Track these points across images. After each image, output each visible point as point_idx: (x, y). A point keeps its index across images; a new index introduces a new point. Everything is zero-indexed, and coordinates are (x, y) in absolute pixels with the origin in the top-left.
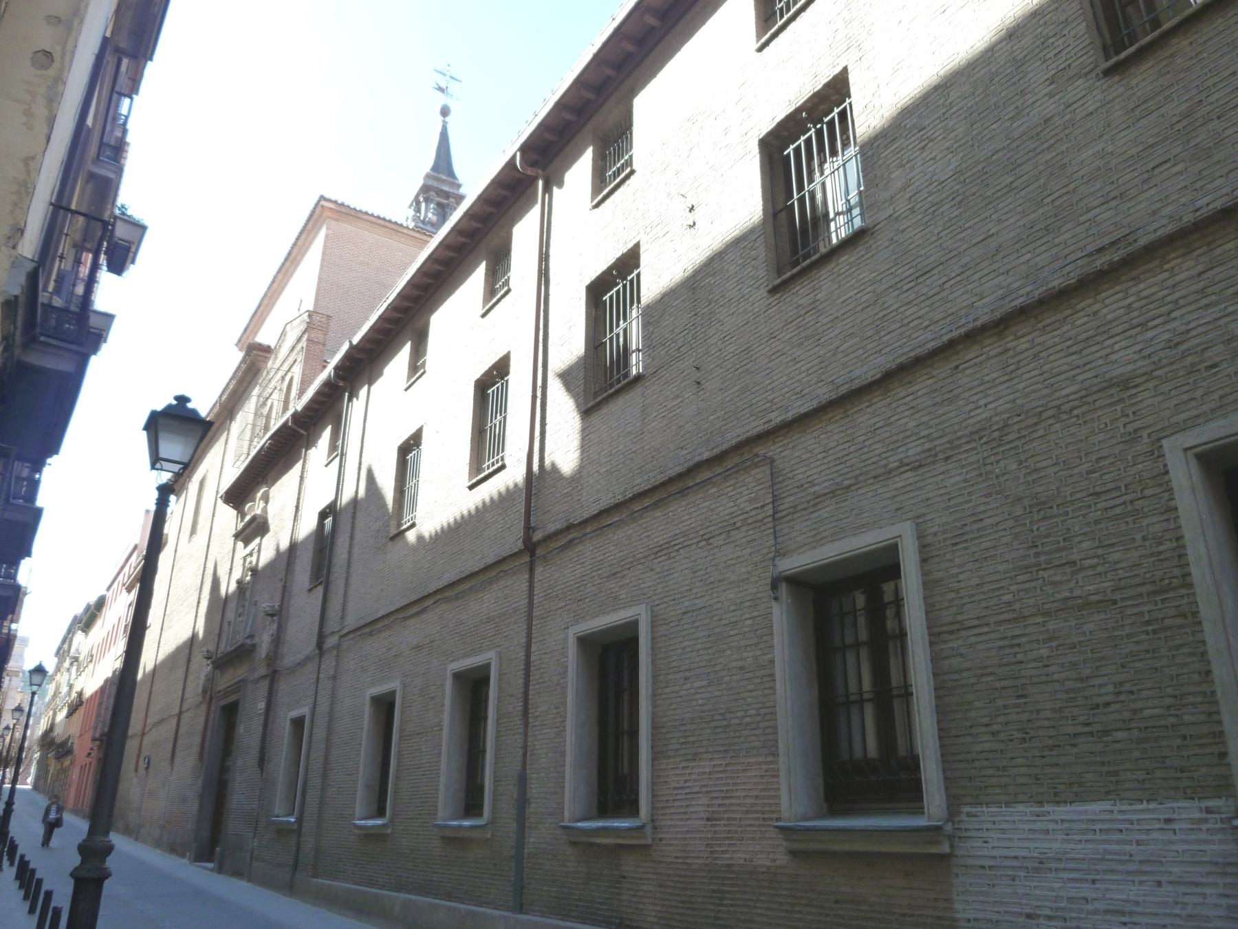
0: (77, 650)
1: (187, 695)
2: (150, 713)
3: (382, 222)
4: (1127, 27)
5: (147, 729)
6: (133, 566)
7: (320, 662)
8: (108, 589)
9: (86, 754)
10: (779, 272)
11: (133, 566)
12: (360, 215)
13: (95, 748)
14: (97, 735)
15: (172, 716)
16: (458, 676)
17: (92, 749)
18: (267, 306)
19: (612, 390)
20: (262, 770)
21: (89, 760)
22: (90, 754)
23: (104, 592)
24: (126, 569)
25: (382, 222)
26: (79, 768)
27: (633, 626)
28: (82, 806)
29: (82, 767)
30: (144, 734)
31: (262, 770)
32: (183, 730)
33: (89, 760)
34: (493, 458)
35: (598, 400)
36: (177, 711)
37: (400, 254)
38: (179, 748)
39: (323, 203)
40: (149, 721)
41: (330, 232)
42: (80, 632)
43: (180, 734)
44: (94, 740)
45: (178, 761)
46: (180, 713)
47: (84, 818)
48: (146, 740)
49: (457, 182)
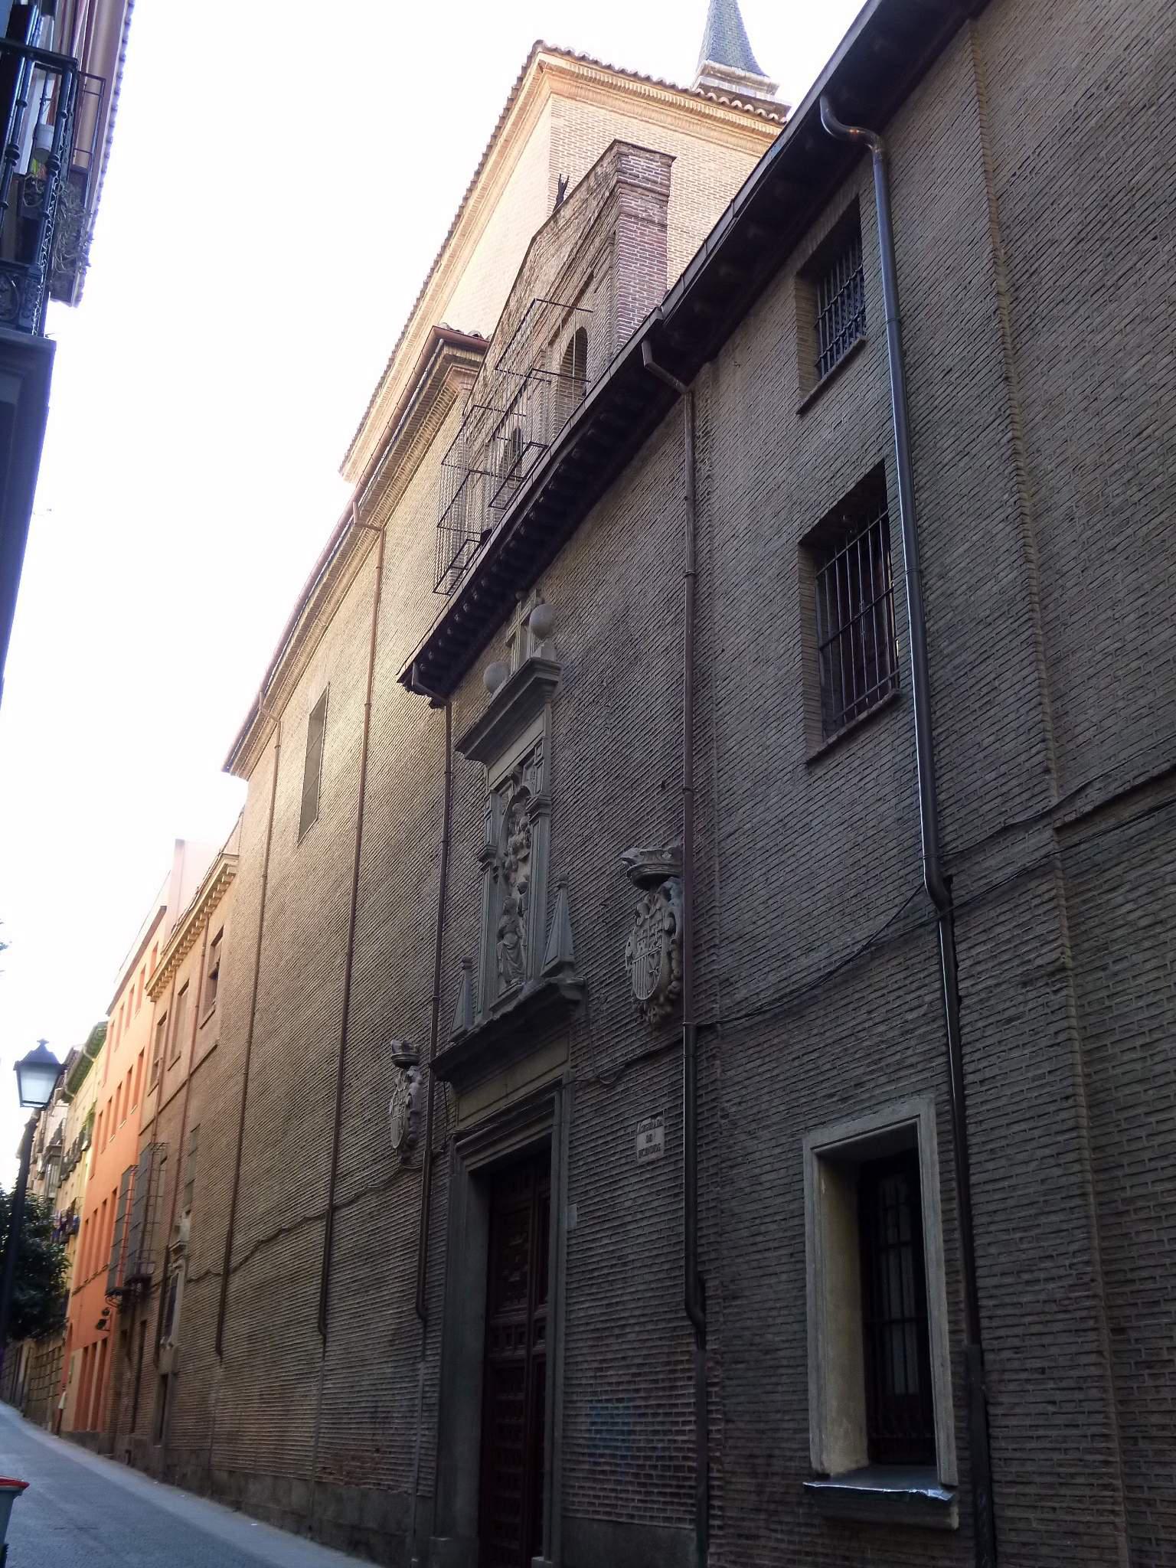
0: (59, 1131)
1: (346, 1163)
2: (241, 1224)
3: (668, 96)
4: (892, 670)
5: (235, 1260)
6: (159, 951)
7: (952, 945)
8: (109, 1013)
9: (97, 1322)
10: (826, 731)
11: (159, 951)
12: (621, 82)
13: (113, 1311)
14: (118, 1283)
15: (307, 1220)
16: (833, 1160)
17: (105, 1313)
18: (438, 285)
19: (864, 715)
20: (700, 1334)
21: (103, 1334)
22: (102, 1323)
23: (105, 1018)
24: (146, 959)
25: (668, 96)
26: (81, 1351)
27: (907, 1135)
28: (94, 1426)
29: (86, 1349)
30: (227, 1273)
31: (700, 1334)
32: (344, 1246)
33: (103, 1334)
34: (860, 692)
35: (831, 740)
36: (321, 1204)
37: (712, 165)
38: (336, 1290)
39: (541, 57)
40: (239, 1240)
41: (561, 122)
42: (60, 1102)
43: (337, 1256)
44: (111, 1293)
45: (337, 1323)
46: (333, 1209)
47: (99, 1453)
48: (236, 1282)
49: (766, 80)
